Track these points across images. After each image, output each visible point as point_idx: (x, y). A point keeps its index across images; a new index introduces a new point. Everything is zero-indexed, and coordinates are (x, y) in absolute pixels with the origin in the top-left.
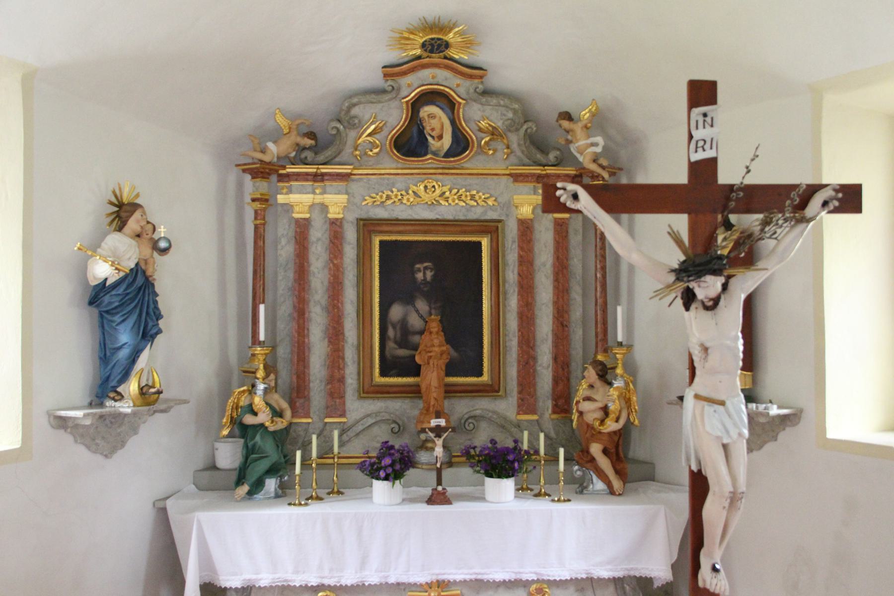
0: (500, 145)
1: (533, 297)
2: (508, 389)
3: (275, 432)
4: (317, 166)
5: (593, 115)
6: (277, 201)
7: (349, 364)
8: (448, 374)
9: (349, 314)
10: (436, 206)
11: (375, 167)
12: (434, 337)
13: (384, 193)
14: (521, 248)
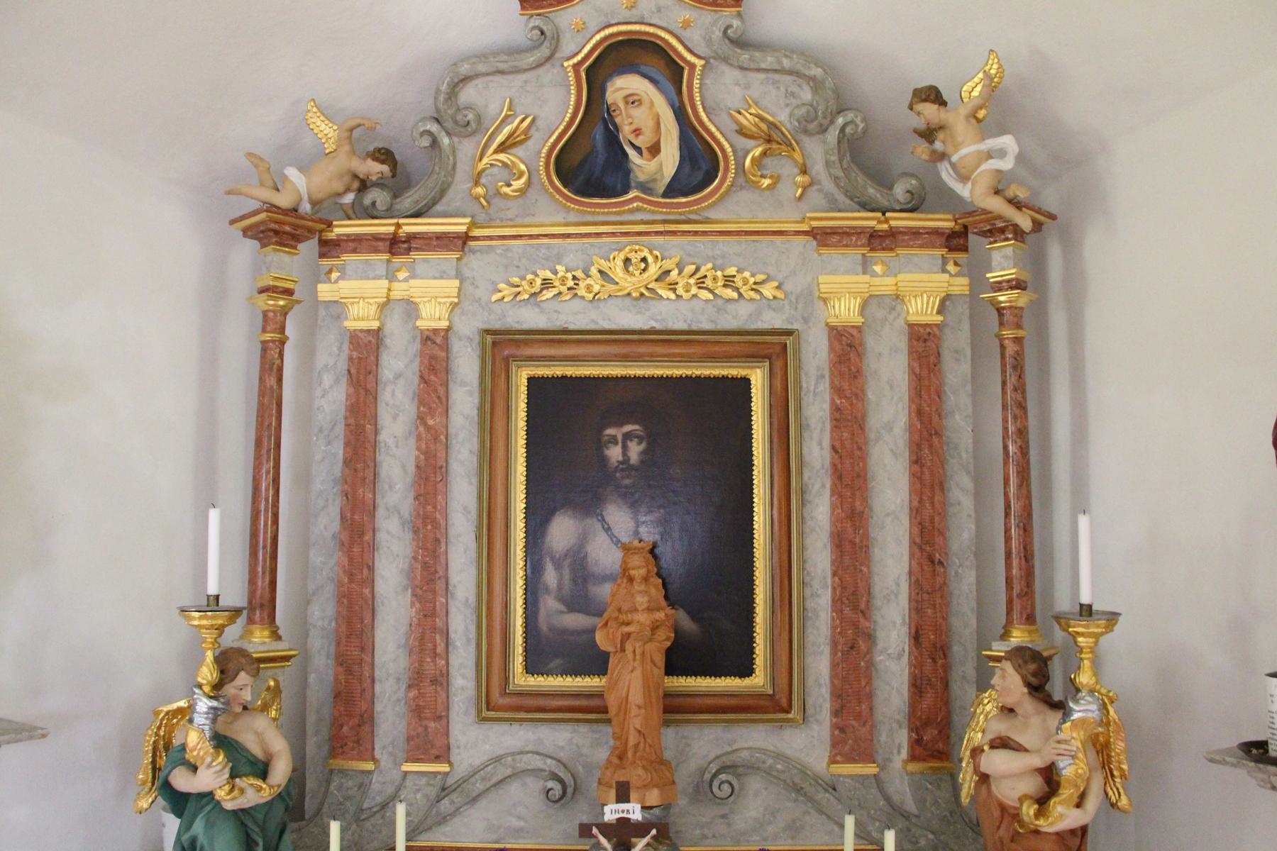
0: (787, 169)
1: (865, 500)
2: (810, 702)
3: (239, 815)
4: (394, 221)
5: (992, 87)
6: (317, 297)
7: (458, 644)
8: (671, 670)
9: (459, 535)
10: (651, 303)
11: (519, 221)
12: (639, 589)
13: (537, 275)
14: (837, 390)
